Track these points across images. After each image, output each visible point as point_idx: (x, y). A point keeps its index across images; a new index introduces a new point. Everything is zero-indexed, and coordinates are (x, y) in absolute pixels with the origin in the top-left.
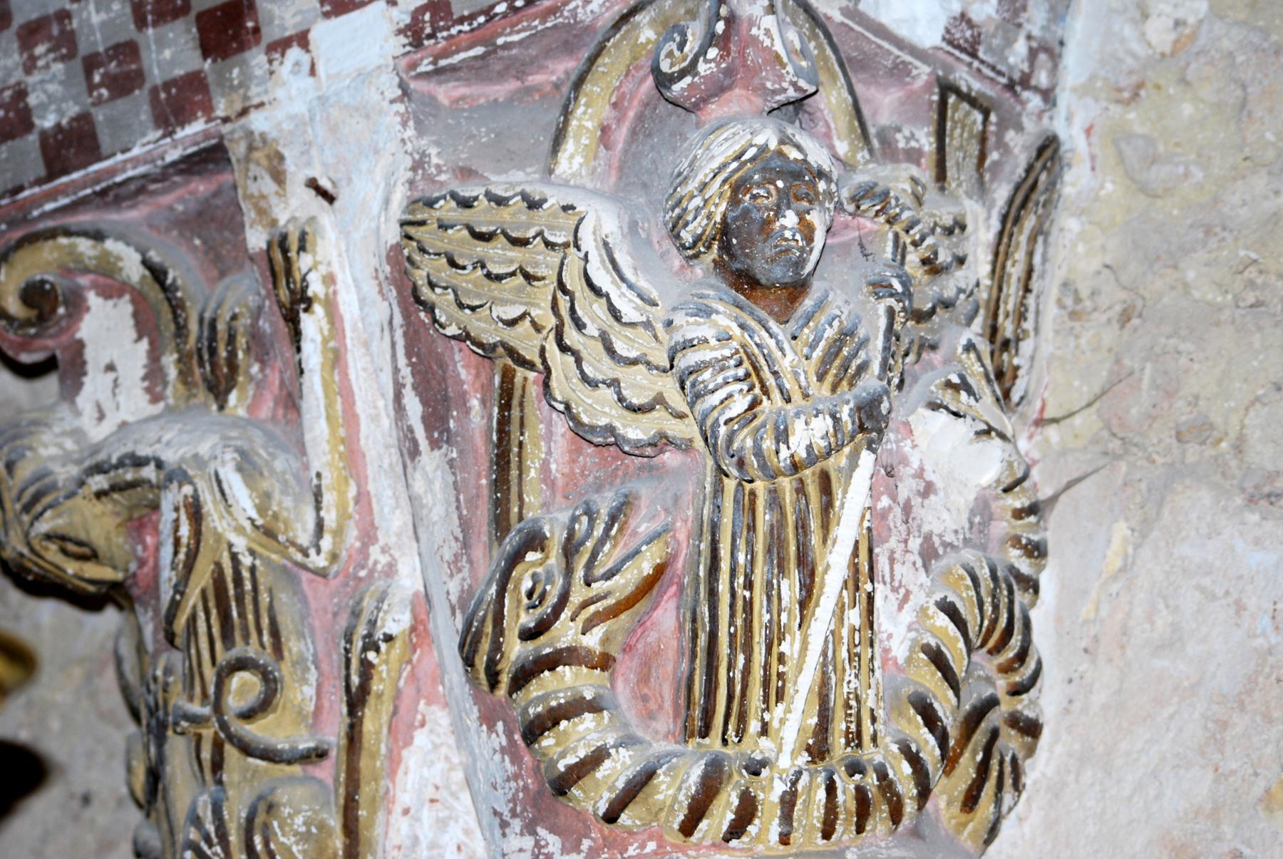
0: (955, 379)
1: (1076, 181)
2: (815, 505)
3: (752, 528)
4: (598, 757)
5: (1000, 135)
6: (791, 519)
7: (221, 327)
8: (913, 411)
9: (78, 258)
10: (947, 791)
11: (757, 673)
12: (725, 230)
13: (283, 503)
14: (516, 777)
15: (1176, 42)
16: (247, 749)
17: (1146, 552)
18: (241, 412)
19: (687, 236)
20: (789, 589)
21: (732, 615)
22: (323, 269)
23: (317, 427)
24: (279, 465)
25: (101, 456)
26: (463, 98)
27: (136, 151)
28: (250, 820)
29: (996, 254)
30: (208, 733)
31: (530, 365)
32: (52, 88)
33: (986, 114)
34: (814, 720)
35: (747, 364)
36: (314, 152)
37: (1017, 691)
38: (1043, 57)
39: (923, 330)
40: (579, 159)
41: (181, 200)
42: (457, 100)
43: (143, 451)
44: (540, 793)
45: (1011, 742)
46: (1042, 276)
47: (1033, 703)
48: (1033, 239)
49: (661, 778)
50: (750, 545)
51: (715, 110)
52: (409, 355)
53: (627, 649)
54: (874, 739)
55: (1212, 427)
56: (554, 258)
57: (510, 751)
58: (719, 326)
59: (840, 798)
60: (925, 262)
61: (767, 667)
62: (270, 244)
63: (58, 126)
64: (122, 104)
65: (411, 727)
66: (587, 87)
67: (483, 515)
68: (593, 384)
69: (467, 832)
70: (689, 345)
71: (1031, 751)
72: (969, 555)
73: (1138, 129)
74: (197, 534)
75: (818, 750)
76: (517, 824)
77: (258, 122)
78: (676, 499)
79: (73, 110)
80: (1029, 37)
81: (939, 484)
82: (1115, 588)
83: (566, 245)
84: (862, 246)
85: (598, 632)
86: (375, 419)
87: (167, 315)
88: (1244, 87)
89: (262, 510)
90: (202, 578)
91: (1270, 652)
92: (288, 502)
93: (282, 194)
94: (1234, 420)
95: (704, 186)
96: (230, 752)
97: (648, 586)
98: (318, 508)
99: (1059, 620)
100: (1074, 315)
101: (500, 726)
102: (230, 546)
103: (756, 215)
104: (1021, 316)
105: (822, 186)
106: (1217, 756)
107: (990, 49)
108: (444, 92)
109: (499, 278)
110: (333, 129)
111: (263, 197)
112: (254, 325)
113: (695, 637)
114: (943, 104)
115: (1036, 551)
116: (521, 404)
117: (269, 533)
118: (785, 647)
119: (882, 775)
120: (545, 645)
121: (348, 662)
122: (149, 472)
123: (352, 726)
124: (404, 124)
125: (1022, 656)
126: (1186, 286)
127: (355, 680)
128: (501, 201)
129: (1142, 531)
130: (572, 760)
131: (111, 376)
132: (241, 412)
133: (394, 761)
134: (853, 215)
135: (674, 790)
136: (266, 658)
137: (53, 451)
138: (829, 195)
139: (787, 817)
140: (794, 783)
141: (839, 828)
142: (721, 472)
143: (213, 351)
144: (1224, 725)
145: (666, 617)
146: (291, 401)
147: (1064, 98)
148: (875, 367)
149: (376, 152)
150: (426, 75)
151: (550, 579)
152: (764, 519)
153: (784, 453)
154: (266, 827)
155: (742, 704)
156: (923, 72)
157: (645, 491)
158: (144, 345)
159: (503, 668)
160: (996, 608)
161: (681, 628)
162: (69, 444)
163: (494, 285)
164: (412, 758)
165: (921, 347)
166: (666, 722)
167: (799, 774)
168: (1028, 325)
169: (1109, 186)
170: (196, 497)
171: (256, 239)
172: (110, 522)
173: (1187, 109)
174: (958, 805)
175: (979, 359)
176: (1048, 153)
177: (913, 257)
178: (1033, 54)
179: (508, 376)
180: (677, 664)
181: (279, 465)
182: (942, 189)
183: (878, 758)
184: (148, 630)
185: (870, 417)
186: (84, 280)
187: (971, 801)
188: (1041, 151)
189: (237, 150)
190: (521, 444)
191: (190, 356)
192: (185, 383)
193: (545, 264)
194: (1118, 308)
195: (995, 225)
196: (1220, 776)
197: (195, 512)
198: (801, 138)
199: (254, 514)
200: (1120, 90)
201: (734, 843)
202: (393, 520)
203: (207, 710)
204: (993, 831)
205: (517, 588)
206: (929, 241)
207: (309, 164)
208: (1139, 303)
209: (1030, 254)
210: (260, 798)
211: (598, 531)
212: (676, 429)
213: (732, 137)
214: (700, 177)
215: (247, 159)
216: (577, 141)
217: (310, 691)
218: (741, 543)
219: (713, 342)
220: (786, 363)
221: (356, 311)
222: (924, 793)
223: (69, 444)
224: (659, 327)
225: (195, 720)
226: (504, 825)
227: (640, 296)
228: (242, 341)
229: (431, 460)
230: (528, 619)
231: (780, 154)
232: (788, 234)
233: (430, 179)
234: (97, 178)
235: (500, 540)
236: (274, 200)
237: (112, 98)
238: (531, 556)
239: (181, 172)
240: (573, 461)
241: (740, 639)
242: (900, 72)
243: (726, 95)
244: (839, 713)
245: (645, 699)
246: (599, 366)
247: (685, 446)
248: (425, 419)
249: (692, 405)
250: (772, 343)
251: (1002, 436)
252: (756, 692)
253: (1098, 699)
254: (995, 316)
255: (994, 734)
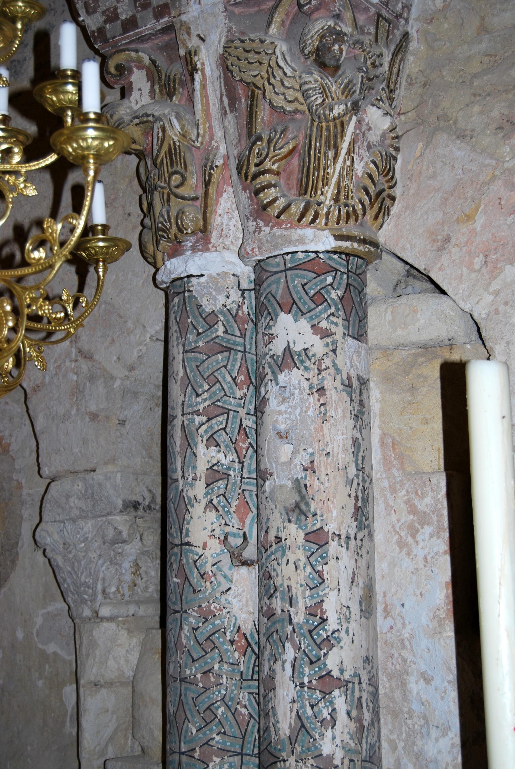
0: (379, 98)
1: (413, 45)
2: (339, 131)
3: (321, 136)
4: (275, 200)
5: (393, 31)
6: (332, 134)
7: (171, 77)
8: (367, 106)
9: (131, 58)
10: (369, 217)
11: (321, 177)
12: (318, 50)
13: (188, 128)
14: (252, 205)
15: (444, 6)
16: (177, 196)
17: (427, 151)
18: (176, 102)
19: (306, 52)
20: (331, 154)
21: (315, 161)
22: (201, 61)
23: (198, 107)
24: (187, 117)
25: (137, 114)
26: (242, 12)
27: (148, 26)
28: (177, 216)
29: (390, 65)
30: (166, 191)
31: (259, 89)
32: (125, 7)
33: (389, 24)
34: (336, 191)
35: (322, 89)
36: (199, 27)
37: (390, 188)
38: (406, 9)
39: (370, 84)
40: (275, 30)
41: (161, 42)
42: (240, 13)
43: (149, 112)
44: (258, 209)
45: (388, 202)
46: (402, 73)
47: (394, 192)
48: (400, 62)
49: (293, 206)
50: (320, 141)
51: (315, 15)
52: (225, 86)
53: (284, 170)
54: (352, 198)
55: (448, 116)
56: (268, 58)
57: (250, 198)
58: (314, 78)
59: (342, 213)
60: (372, 64)
61: (323, 176)
62: (186, 53)
63: (126, 18)
64: (144, 12)
65: (222, 192)
66: (278, 9)
67: (244, 132)
68: (278, 94)
69: (237, 221)
70: (306, 83)
71: (393, 205)
72: (379, 148)
73: (431, 31)
74: (164, 135)
75: (337, 200)
76: (251, 219)
77: (184, 18)
78: (300, 128)
79: (130, 14)
80: (402, 3)
81: (373, 128)
82: (418, 161)
83: (271, 54)
84: (355, 58)
85: (276, 165)
86: (214, 105)
87: (156, 74)
88: (463, 19)
89: (182, 129)
90: (165, 148)
91: (461, 179)
92: (189, 127)
93: (190, 39)
94: (454, 115)
95: (312, 37)
96: (172, 196)
97: (291, 152)
98: (198, 130)
99: (402, 170)
100: (410, 84)
101: (248, 191)
102: (173, 139)
103: (327, 45)
104: (396, 83)
105: (346, 38)
106: (444, 208)
107: (392, 5)
108: (237, 10)
109: (252, 63)
110: (205, 20)
111: (185, 40)
112: (181, 77)
113: (303, 167)
114: (378, 19)
115: (397, 149)
116: (257, 100)
117: (184, 136)
118: (329, 170)
119: (354, 208)
120: (261, 168)
121: (205, 173)
122: (151, 118)
123: (206, 191)
124: (225, 19)
125: (392, 178)
126: (443, 76)
127: (207, 178)
128: (253, 41)
129: (426, 146)
130: (268, 200)
131: (140, 92)
132: (176, 102)
133: (217, 201)
134: (353, 49)
135: (296, 209)
136: (183, 171)
137: (123, 112)
138: (347, 41)
139: (327, 218)
140: (330, 209)
141: (341, 222)
142: (313, 120)
143: (169, 84)
144: (447, 200)
145: (295, 161)
146: (191, 99)
147: (411, 22)
148: (358, 92)
149: (217, 27)
150: (232, 5)
151: (263, 149)
152: (325, 134)
153: (331, 115)
154: (182, 218)
155: (316, 186)
156: (373, 10)
157: (291, 126)
158: (149, 83)
159: (249, 174)
160: (386, 163)
161: (299, 165)
162: (128, 111)
163: (250, 65)
164: (222, 201)
165: (370, 89)
166: (294, 191)
167: (331, 206)
168: (398, 86)
169: (422, 47)
170: (164, 125)
171: (182, 52)
172: (139, 133)
173: (446, 26)
174: (373, 218)
175: (385, 93)
176: (406, 37)
177: (369, 62)
178: (403, 8)
179: (253, 92)
180: (298, 175)
181: (187, 117)
182: (377, 45)
183: (353, 203)
184: (149, 164)
185: (356, 106)
186: (132, 64)
187: (376, 217)
188: (404, 36)
189: (177, 26)
190: (256, 112)
191: (162, 86)
192: (161, 94)
193: (265, 59)
194: (423, 83)
195: (390, 56)
196: (445, 214)
197: (164, 130)
198: (340, 24)
199: (180, 130)
200: (427, 20)
201: (312, 225)
202: (219, 134)
203: (166, 185)
204: (381, 226)
205: (254, 152)
206: (373, 58)
207: (198, 30)
208: (429, 81)
209: (399, 66)
210: (180, 210)
211: (277, 137)
212: (300, 107)
213: (319, 25)
214: (311, 34)
215: (180, 29)
216: (275, 25)
217: (194, 181)
218: (318, 140)
219: (313, 82)
220: (333, 89)
221: (210, 74)
222: (364, 214)
223: (128, 111)
224: (297, 78)
225: (162, 188)
226: (248, 219)
227: (292, 69)
228: (177, 82)
229: (230, 116)
230: (256, 161)
231: (334, 28)
232: (336, 51)
233: (232, 35)
234: (137, 34)
235: (250, 139)
236: (187, 41)
237: (142, 10)
238: (258, 143)
239: (161, 33)
240: (271, 117)
241: (316, 168)
242: (367, 9)
243: (319, 11)
244: (343, 190)
245: (288, 184)
246: (279, 89)
247: (303, 113)
248: (229, 104)
249: (305, 101)
250: (329, 83)
251: (391, 115)
252: (320, 183)
253: (412, 191)
254: (389, 83)
255: (384, 199)
